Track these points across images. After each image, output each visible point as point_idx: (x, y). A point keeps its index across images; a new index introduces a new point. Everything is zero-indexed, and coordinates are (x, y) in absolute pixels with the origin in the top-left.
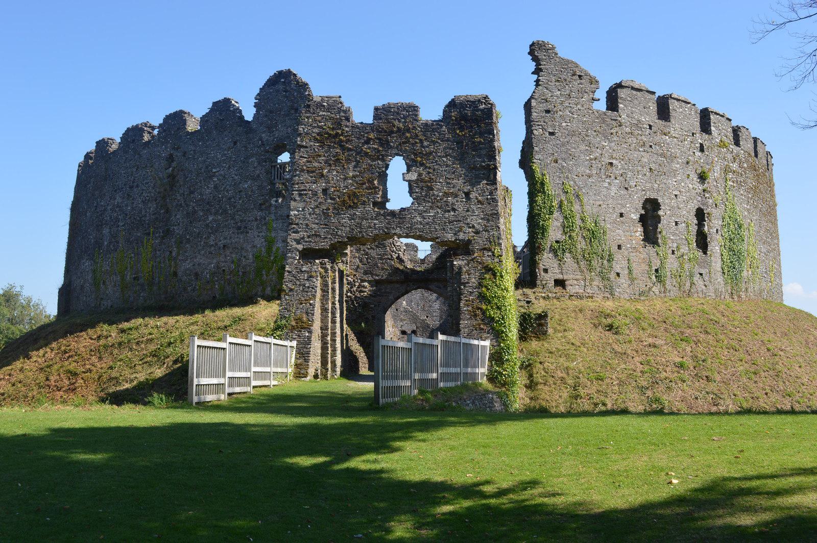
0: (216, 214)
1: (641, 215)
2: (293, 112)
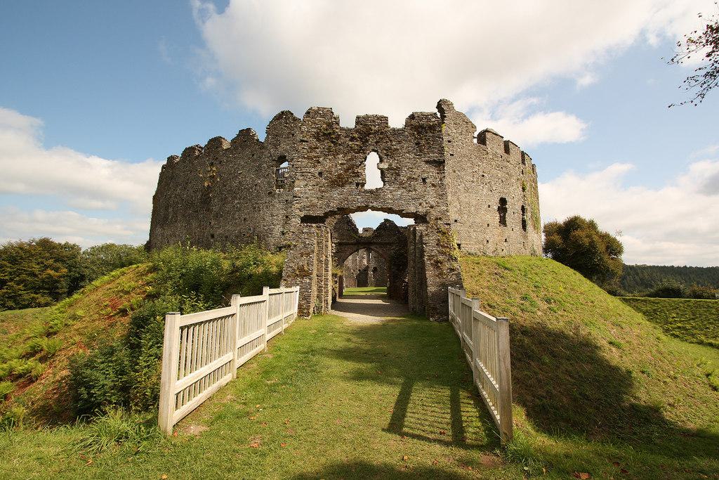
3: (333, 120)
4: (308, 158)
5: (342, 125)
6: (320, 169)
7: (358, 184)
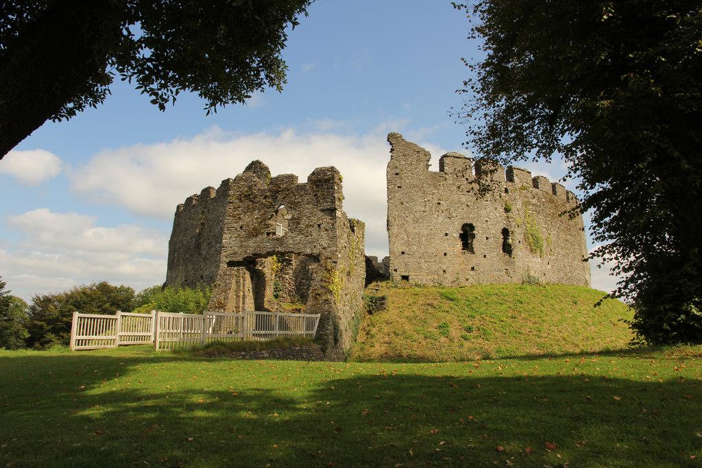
1: (461, 234)
6: (241, 223)
7: (268, 234)
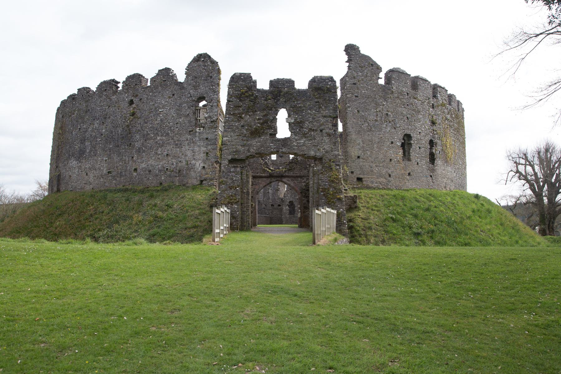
0: (162, 136)
1: (402, 143)
2: (209, 78)
3: (252, 84)
4: (234, 114)
5: (259, 87)
